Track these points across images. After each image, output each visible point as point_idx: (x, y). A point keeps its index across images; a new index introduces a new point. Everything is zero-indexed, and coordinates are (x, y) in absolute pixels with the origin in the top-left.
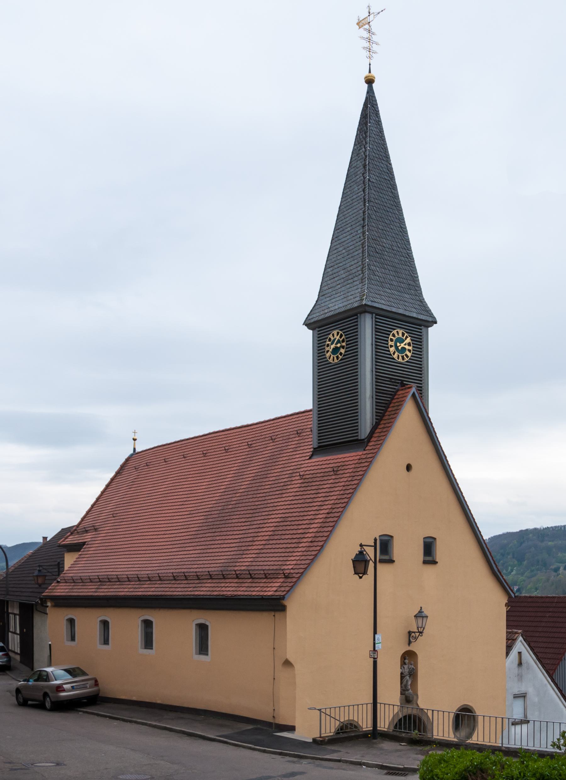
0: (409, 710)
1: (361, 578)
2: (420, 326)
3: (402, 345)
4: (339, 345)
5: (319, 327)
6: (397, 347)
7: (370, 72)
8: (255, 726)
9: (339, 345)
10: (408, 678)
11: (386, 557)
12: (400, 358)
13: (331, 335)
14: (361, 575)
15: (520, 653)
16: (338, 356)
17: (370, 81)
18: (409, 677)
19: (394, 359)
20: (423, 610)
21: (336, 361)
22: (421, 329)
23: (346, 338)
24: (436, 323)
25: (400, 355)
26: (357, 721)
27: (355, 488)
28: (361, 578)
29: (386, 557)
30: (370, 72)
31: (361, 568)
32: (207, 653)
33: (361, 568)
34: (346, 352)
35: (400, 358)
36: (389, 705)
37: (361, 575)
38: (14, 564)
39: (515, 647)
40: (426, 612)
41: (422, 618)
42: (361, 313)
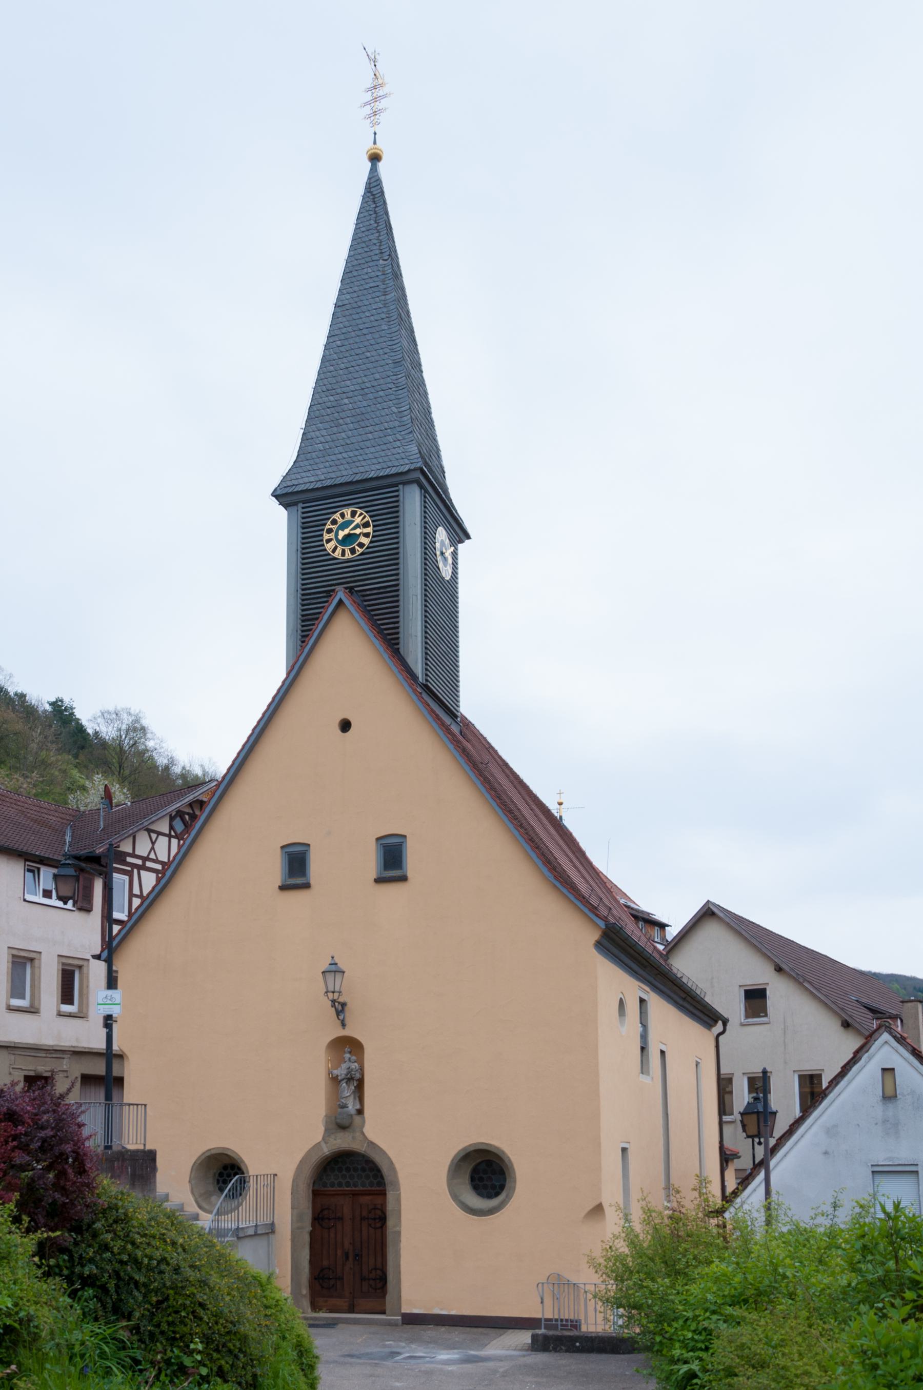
0: (342, 1142)
2: (396, 485)
4: (358, 531)
7: (375, 143)
9: (358, 531)
10: (344, 1084)
11: (299, 881)
12: (348, 552)
13: (338, 514)
15: (888, 1071)
16: (354, 547)
17: (375, 158)
18: (347, 1083)
19: (335, 559)
20: (337, 960)
21: (348, 555)
27: (521, 782)
29: (299, 881)
30: (375, 143)
34: (371, 542)
35: (348, 552)
36: (137, 1105)
38: (23, 1089)
39: (870, 1059)
40: (341, 966)
41: (333, 974)
42: (405, 483)
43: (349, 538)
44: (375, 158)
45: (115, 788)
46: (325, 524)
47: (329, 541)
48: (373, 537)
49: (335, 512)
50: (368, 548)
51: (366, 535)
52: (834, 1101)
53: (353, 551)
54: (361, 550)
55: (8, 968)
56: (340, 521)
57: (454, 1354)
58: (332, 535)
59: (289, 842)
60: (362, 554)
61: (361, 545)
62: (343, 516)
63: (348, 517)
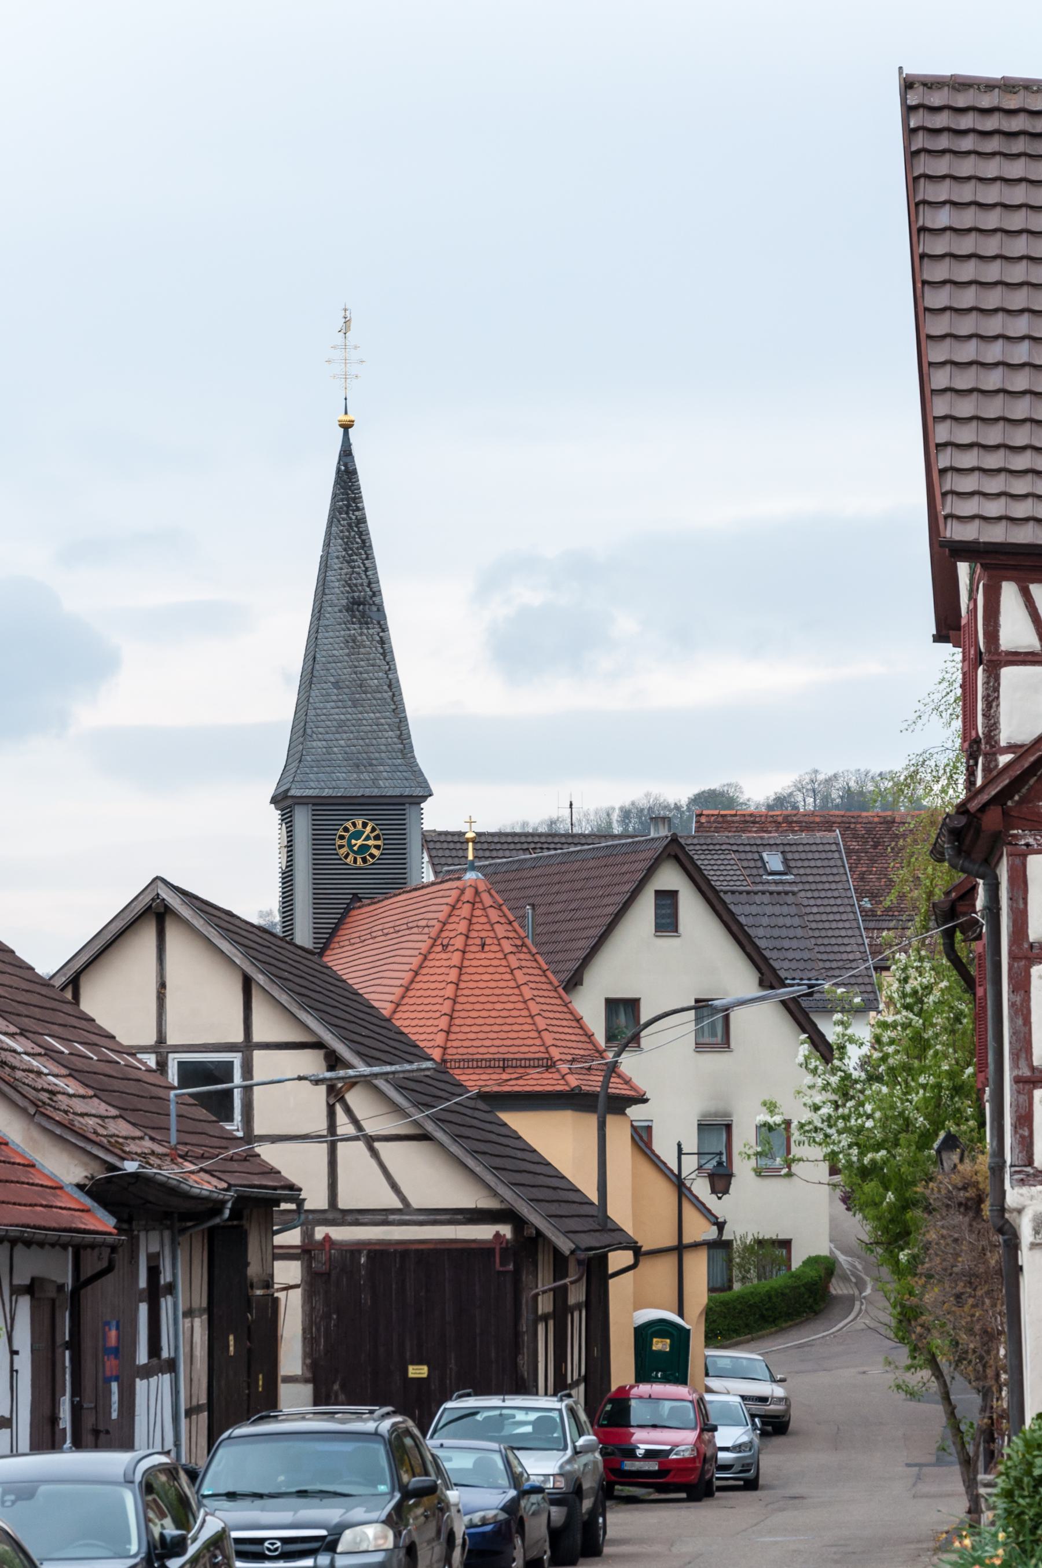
1: (720, 1198)
2: (403, 804)
3: (359, 842)
4: (370, 843)
5: (314, 804)
6: (351, 846)
8: (459, 1541)
12: (359, 861)
14: (720, 1195)
17: (346, 427)
19: (346, 864)
22: (404, 810)
23: (334, 839)
24: (431, 795)
25: (358, 857)
26: (397, 1204)
28: (720, 1198)
31: (720, 1184)
32: (88, 1438)
33: (720, 1184)
34: (382, 854)
35: (359, 861)
37: (720, 1195)
43: (364, 848)
44: (346, 427)
45: (429, 1064)
46: (338, 830)
47: (341, 847)
48: (384, 849)
49: (348, 820)
50: (378, 859)
51: (377, 847)
52: (463, 1125)
53: (364, 860)
54: (372, 861)
55: (62, 1181)
56: (352, 829)
57: (629, 1491)
58: (344, 842)
59: (705, 1202)
60: (373, 864)
61: (372, 856)
62: (354, 825)
63: (360, 827)
